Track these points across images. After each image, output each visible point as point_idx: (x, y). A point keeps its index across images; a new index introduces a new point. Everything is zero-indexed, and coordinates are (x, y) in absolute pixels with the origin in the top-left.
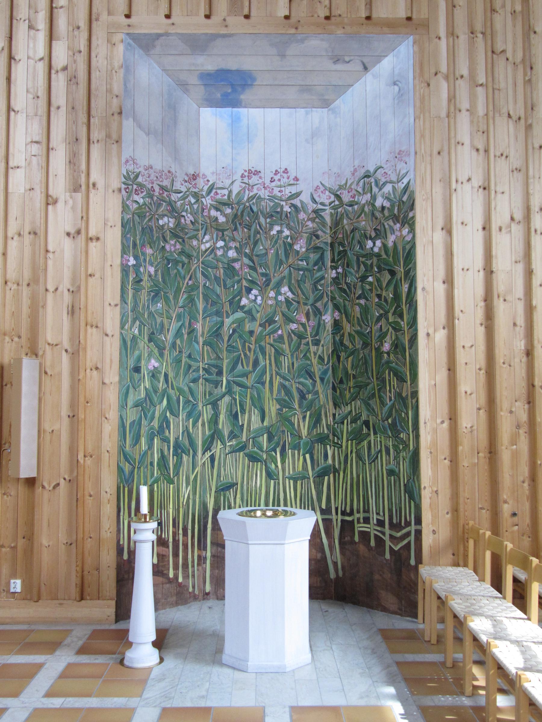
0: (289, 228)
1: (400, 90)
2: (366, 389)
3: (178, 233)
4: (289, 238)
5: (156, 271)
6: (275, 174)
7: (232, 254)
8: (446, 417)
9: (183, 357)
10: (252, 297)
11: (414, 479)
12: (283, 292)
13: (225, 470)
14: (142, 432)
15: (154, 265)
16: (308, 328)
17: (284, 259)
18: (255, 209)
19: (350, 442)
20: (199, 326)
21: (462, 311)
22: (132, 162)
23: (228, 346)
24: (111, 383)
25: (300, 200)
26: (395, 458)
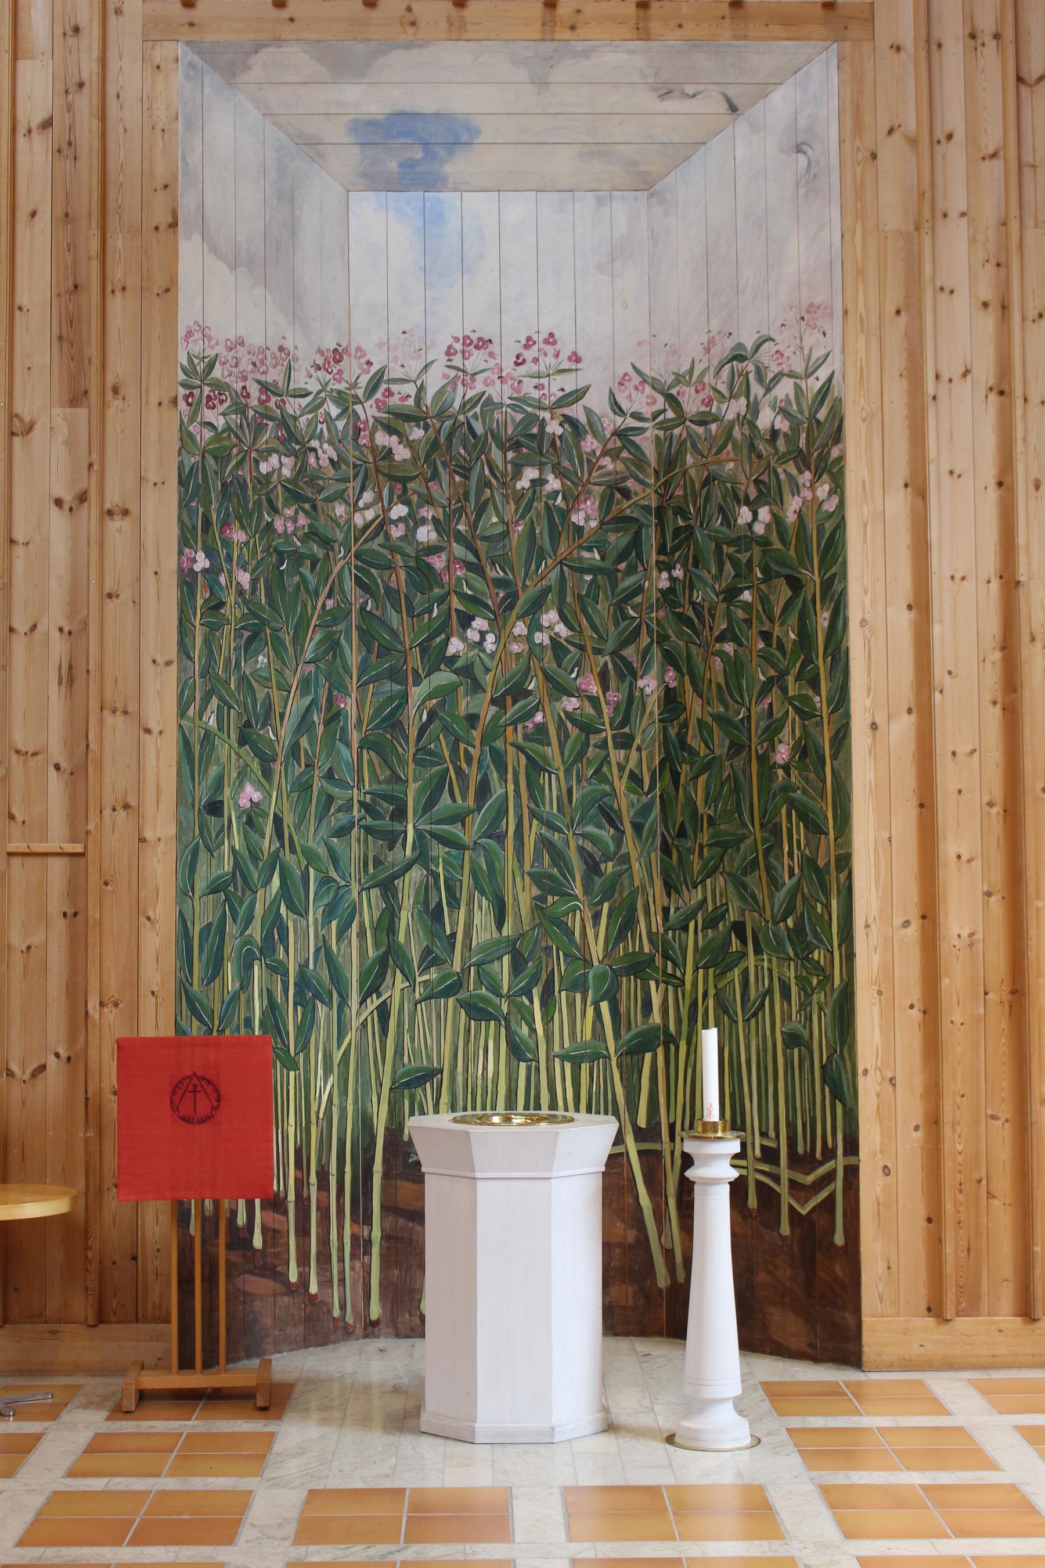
0: (560, 472)
1: (809, 163)
2: (738, 849)
3: (301, 490)
4: (560, 497)
5: (254, 582)
6: (527, 347)
7: (425, 534)
8: (914, 914)
9: (316, 778)
10: (473, 635)
11: (841, 1051)
12: (546, 624)
13: (412, 1039)
14: (227, 950)
15: (250, 567)
16: (605, 709)
17: (547, 545)
18: (479, 429)
19: (701, 971)
20: (349, 705)
21: (950, 673)
22: (200, 335)
23: (418, 751)
24: (159, 839)
25: (585, 407)
26: (802, 1006)
